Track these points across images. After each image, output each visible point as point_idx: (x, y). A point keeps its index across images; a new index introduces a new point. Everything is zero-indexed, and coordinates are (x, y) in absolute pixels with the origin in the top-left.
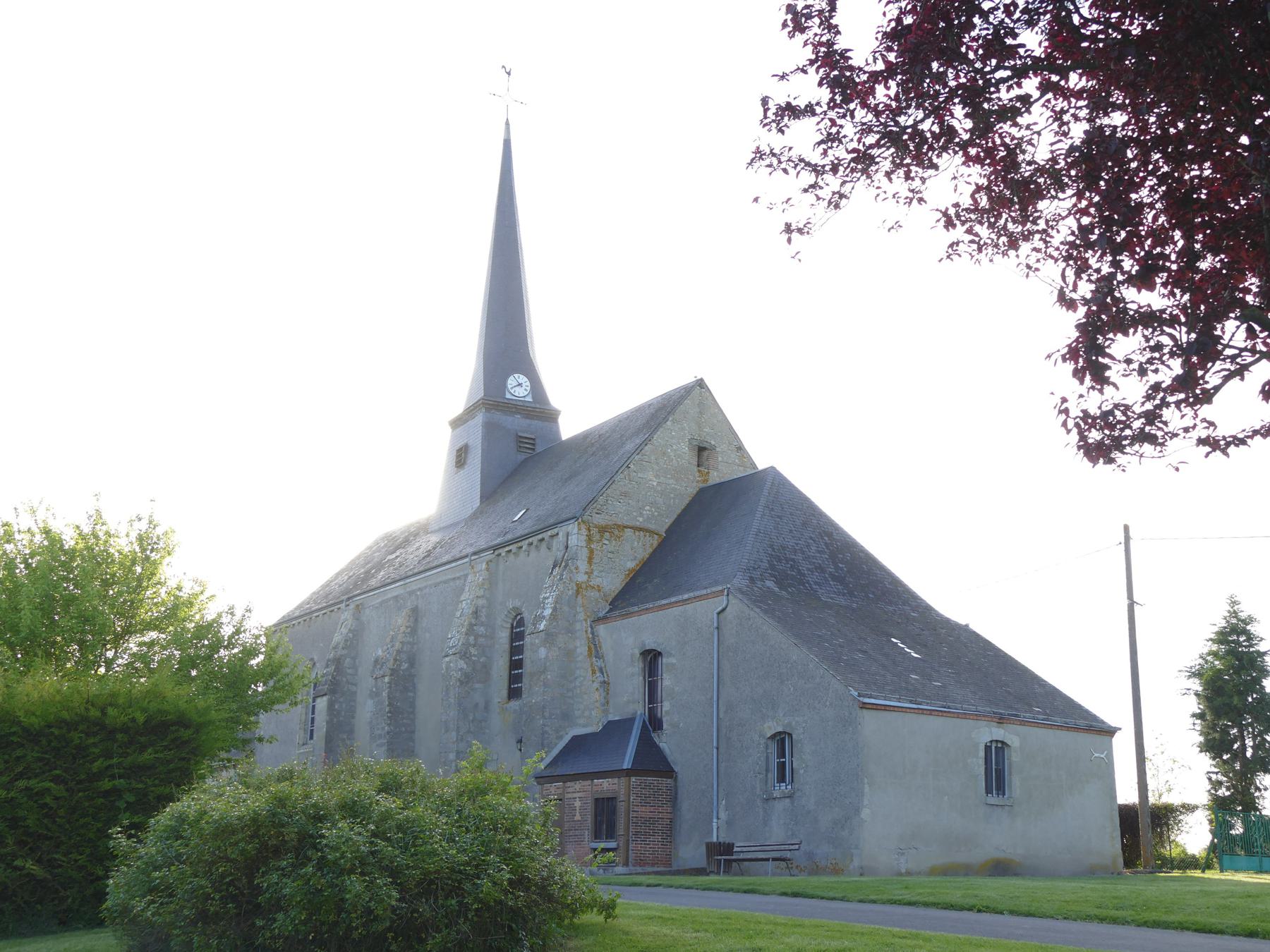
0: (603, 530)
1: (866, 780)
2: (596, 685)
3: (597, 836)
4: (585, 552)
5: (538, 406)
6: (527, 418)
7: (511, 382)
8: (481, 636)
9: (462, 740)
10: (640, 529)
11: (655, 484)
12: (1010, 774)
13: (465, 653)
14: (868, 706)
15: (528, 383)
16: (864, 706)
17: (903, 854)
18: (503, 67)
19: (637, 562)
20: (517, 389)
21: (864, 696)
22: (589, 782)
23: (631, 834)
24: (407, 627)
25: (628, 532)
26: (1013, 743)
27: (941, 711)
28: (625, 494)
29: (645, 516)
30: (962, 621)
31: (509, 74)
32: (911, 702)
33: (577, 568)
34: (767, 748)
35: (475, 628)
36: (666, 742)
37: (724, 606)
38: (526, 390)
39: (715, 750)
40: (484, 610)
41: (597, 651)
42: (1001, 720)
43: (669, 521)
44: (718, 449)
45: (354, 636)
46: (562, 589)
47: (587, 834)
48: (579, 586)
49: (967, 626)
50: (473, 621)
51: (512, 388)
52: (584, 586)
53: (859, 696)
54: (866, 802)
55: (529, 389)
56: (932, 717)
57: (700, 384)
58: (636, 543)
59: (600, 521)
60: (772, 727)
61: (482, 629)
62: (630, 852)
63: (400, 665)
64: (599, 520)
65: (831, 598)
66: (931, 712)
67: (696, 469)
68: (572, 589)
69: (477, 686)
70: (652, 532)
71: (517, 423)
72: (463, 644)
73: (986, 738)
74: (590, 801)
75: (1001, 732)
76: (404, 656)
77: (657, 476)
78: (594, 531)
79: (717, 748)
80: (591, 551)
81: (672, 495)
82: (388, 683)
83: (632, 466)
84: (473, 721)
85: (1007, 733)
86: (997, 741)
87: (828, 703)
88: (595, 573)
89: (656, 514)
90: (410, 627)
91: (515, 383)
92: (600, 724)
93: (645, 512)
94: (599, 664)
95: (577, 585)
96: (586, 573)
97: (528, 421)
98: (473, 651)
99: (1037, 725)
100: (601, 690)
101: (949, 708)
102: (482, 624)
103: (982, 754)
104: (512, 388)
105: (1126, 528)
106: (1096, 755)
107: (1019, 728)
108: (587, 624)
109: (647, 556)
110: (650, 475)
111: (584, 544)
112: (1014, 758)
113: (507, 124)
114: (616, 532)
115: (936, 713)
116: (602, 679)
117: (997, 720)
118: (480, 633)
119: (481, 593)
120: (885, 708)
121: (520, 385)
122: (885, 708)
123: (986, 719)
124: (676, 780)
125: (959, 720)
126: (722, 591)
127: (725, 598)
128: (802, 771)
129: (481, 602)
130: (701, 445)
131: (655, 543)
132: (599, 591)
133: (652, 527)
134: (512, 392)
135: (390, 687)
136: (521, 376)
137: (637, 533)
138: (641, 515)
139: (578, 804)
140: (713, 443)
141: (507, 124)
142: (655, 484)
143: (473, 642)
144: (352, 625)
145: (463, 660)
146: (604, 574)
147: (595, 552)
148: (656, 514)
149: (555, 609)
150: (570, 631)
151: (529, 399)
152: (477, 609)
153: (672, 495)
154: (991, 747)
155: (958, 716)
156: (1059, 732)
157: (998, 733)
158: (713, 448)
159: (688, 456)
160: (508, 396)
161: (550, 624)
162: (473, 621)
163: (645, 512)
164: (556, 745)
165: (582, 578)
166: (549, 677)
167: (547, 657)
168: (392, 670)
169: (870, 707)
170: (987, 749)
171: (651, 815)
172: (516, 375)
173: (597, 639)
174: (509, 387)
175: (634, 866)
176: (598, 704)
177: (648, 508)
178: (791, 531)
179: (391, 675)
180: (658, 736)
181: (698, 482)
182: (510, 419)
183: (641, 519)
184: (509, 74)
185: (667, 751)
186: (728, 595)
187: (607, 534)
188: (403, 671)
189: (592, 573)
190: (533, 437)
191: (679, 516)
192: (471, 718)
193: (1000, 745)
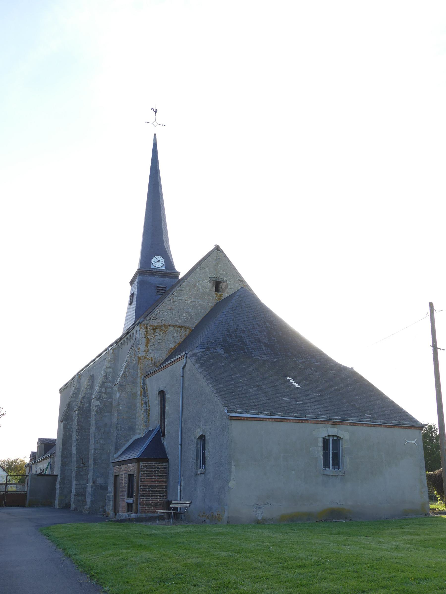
0: (155, 328)
1: (233, 463)
2: (143, 411)
3: (128, 496)
4: (144, 340)
5: (168, 271)
6: (162, 277)
7: (154, 260)
8: (109, 388)
9: (97, 443)
10: (179, 327)
11: (189, 302)
12: (343, 456)
13: (100, 397)
14: (234, 418)
15: (163, 260)
16: (231, 418)
17: (260, 508)
18: (152, 109)
19: (176, 344)
20: (157, 263)
21: (231, 412)
22: (126, 466)
23: (139, 495)
24: (88, 385)
25: (171, 329)
27: (289, 419)
28: (170, 309)
29: (183, 320)
30: (349, 365)
31: (156, 112)
32: (267, 414)
33: (139, 349)
34: (197, 444)
35: (105, 384)
36: (166, 442)
37: (184, 363)
38: (162, 263)
39: (180, 446)
40: (111, 374)
41: (145, 393)
42: (335, 423)
43: (197, 322)
44: (227, 282)
45: (77, 391)
46: (129, 360)
47: (126, 496)
48: (140, 358)
49: (352, 368)
50: (104, 380)
51: (154, 263)
52: (142, 358)
53: (228, 412)
54: (232, 476)
55: (163, 263)
56: (282, 423)
57: (217, 248)
58: (176, 334)
59: (155, 323)
60: (199, 433)
61: (110, 384)
62: (139, 505)
63: (84, 405)
64: (153, 323)
65: (261, 357)
66: (281, 420)
67: (214, 293)
68: (136, 360)
69: (106, 414)
70: (185, 328)
71: (157, 280)
72: (99, 392)
73: (325, 434)
74: (127, 476)
76: (86, 400)
77: (190, 298)
78: (150, 329)
79: (181, 445)
80: (148, 340)
81: (199, 308)
82: (77, 414)
83: (175, 293)
84: (104, 433)
86: (333, 436)
87: (218, 418)
88: (150, 351)
89: (189, 318)
90: (89, 385)
91: (156, 261)
92: (144, 433)
93: (182, 318)
94: (145, 400)
95: (139, 358)
96: (145, 351)
97: (162, 279)
98: (104, 396)
99: (363, 425)
100: (145, 414)
101: (295, 417)
102: (110, 382)
103: (321, 444)
105: (431, 305)
106: (409, 441)
107: (350, 428)
108: (141, 378)
109: (182, 341)
110: (186, 298)
111: (143, 336)
112: (345, 445)
113: (155, 136)
114: (163, 329)
115: (286, 420)
116: (145, 408)
117: (332, 423)
118: (108, 386)
119: (110, 365)
120: (247, 419)
121: (159, 261)
122: (247, 419)
123: (324, 423)
124: (168, 464)
125: (303, 424)
126: (184, 356)
127: (184, 359)
128: (208, 458)
129: (109, 370)
130: (217, 280)
131: (187, 334)
132: (152, 360)
133: (187, 325)
134: (155, 265)
135: (78, 416)
136: (159, 257)
137: (176, 329)
138: (180, 319)
139: (123, 477)
140: (225, 279)
141: (155, 136)
142: (189, 302)
143: (104, 391)
144: (76, 386)
145: (99, 401)
146: (155, 351)
147: (150, 340)
148: (189, 318)
149: (125, 371)
150: (134, 382)
151: (164, 268)
152: (107, 374)
153: (199, 308)
154: (328, 440)
155: (302, 422)
156: (379, 429)
157: (333, 431)
158: (225, 281)
159: (210, 287)
160: (152, 267)
161: (122, 379)
162: (104, 380)
163: (182, 318)
164: (124, 444)
165: (142, 354)
166: (121, 408)
167: (119, 398)
168: (79, 407)
169: (236, 418)
170: (325, 442)
171: (153, 484)
172: (157, 257)
173: (145, 386)
174: (153, 262)
175: (141, 513)
176: (143, 422)
177: (184, 315)
178: (244, 321)
179: (79, 410)
180: (163, 438)
181: (215, 300)
182: (153, 278)
183: (180, 321)
184: (156, 112)
185: (166, 447)
186: (186, 358)
187: (158, 330)
188: (85, 407)
189: (148, 351)
190: (165, 286)
191: (203, 318)
192: (103, 431)
193: (335, 438)
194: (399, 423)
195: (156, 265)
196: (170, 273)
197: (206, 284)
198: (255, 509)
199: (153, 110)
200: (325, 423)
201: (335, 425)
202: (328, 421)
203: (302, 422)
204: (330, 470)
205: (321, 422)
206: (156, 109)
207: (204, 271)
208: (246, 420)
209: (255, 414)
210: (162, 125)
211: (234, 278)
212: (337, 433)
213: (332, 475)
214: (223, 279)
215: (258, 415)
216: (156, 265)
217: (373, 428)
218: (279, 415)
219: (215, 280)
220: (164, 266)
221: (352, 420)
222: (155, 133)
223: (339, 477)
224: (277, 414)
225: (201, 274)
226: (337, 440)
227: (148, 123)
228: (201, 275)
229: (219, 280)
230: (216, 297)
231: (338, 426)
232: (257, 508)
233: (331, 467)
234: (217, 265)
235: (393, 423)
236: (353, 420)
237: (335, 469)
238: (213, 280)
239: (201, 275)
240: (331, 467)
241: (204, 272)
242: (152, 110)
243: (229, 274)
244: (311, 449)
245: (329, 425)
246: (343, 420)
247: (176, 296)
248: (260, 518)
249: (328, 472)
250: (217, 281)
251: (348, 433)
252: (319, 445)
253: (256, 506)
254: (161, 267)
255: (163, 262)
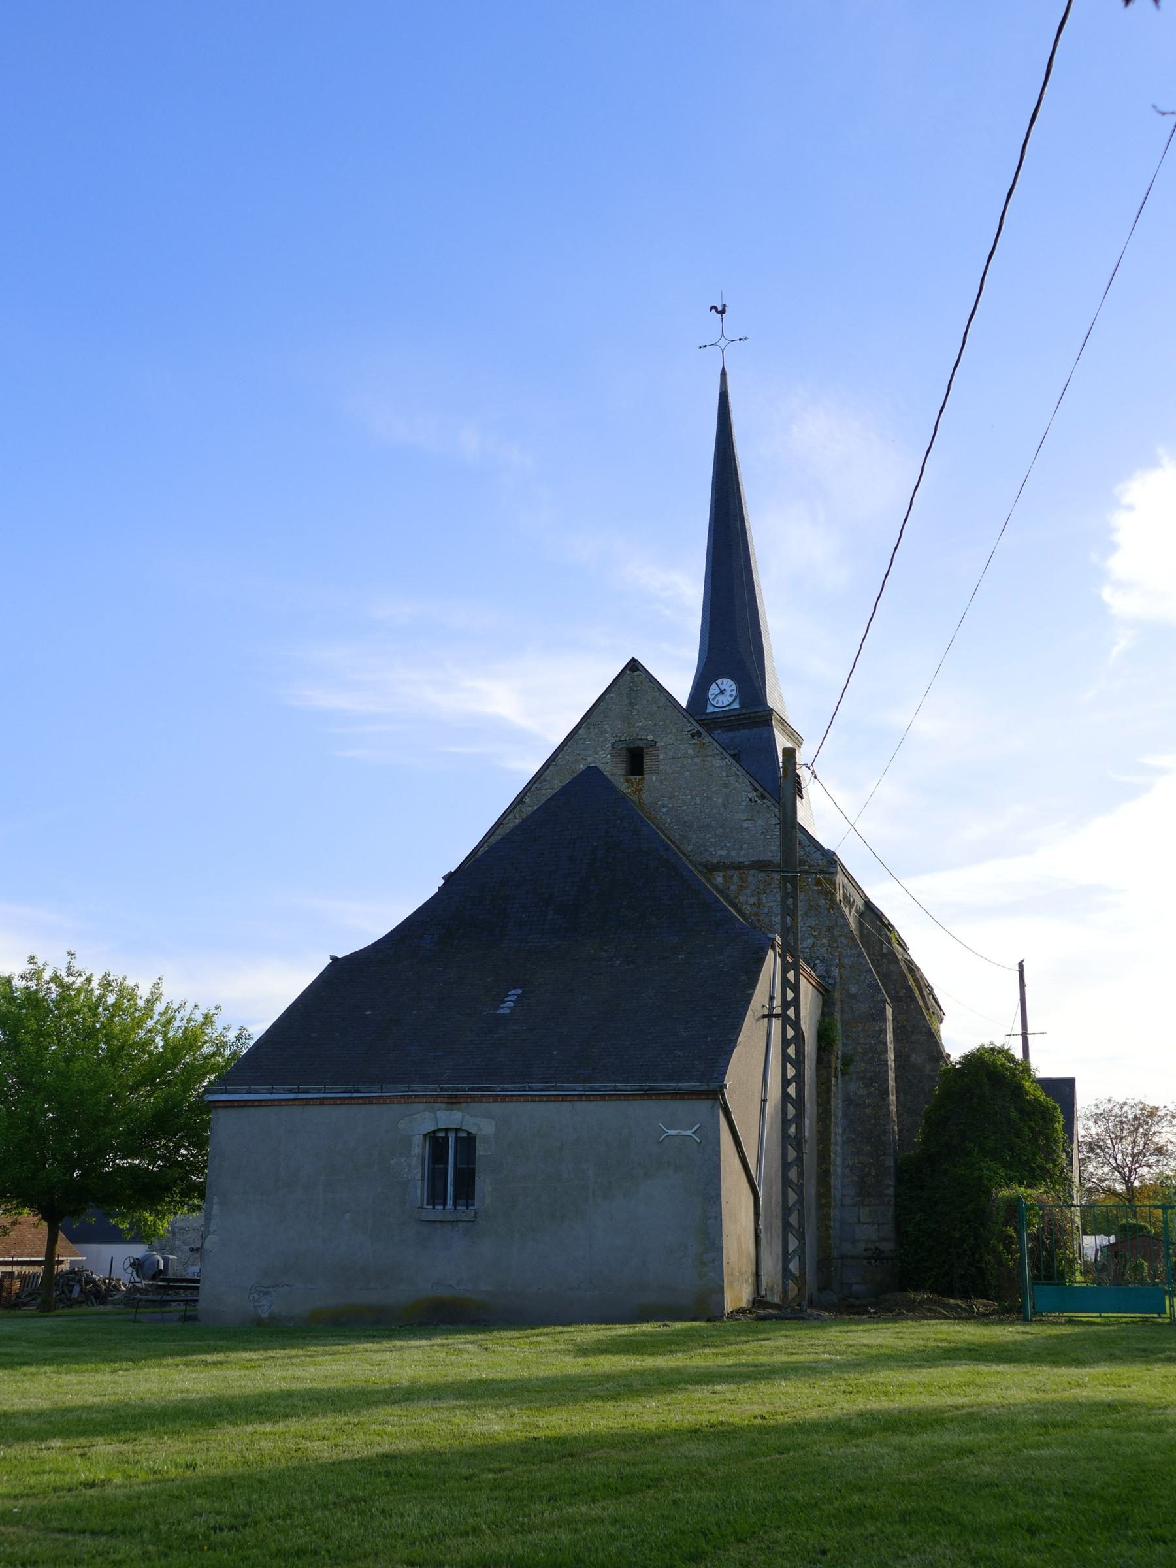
17: (266, 1293)
20: (720, 698)
26: (480, 1129)
27: (340, 1098)
32: (290, 1091)
38: (731, 696)
42: (453, 1100)
51: (713, 699)
55: (734, 693)
66: (321, 1102)
75: (457, 1115)
85: (467, 1117)
86: (457, 1130)
97: (731, 734)
101: (358, 1091)
104: (713, 699)
107: (496, 1108)
113: (723, 374)
117: (446, 1100)
121: (722, 692)
130: (631, 746)
134: (714, 703)
136: (725, 680)
140: (650, 738)
141: (723, 374)
151: (736, 706)
156: (581, 1106)
157: (448, 1118)
160: (710, 709)
174: (711, 698)
194: (637, 1087)
195: (717, 703)
196: (747, 715)
197: (603, 760)
198: (256, 1296)
199: (713, 310)
200: (429, 1100)
201: (455, 1103)
202: (527, 1089)
203: (371, 1103)
204: (444, 1209)
205: (417, 1100)
206: (725, 305)
207: (597, 730)
208: (230, 1107)
209: (264, 1091)
210: (740, 340)
211: (674, 731)
212: (462, 1123)
213: (441, 1222)
214: (647, 740)
215: (272, 1093)
216: (717, 703)
217: (566, 1106)
218: (319, 1091)
219: (624, 746)
220: (737, 701)
221: (529, 1087)
222: (723, 368)
223: (460, 1225)
224: (314, 1089)
225: (589, 740)
226: (468, 1143)
227: (705, 346)
228: (589, 742)
229: (634, 744)
230: (628, 788)
231: (464, 1105)
232: (261, 1294)
233: (450, 1202)
234: (630, 708)
235: (620, 1088)
236: (504, 1090)
237: (458, 1208)
238: (621, 746)
239: (589, 742)
240: (450, 1202)
241: (596, 734)
242: (711, 310)
243: (661, 723)
244: (392, 1162)
245: (438, 1105)
246: (479, 1089)
247: (529, 806)
248: (265, 1315)
249: (437, 1213)
250: (632, 749)
251: (491, 1120)
252: (413, 1153)
253: (258, 1289)
254: (728, 705)
255: (733, 690)
